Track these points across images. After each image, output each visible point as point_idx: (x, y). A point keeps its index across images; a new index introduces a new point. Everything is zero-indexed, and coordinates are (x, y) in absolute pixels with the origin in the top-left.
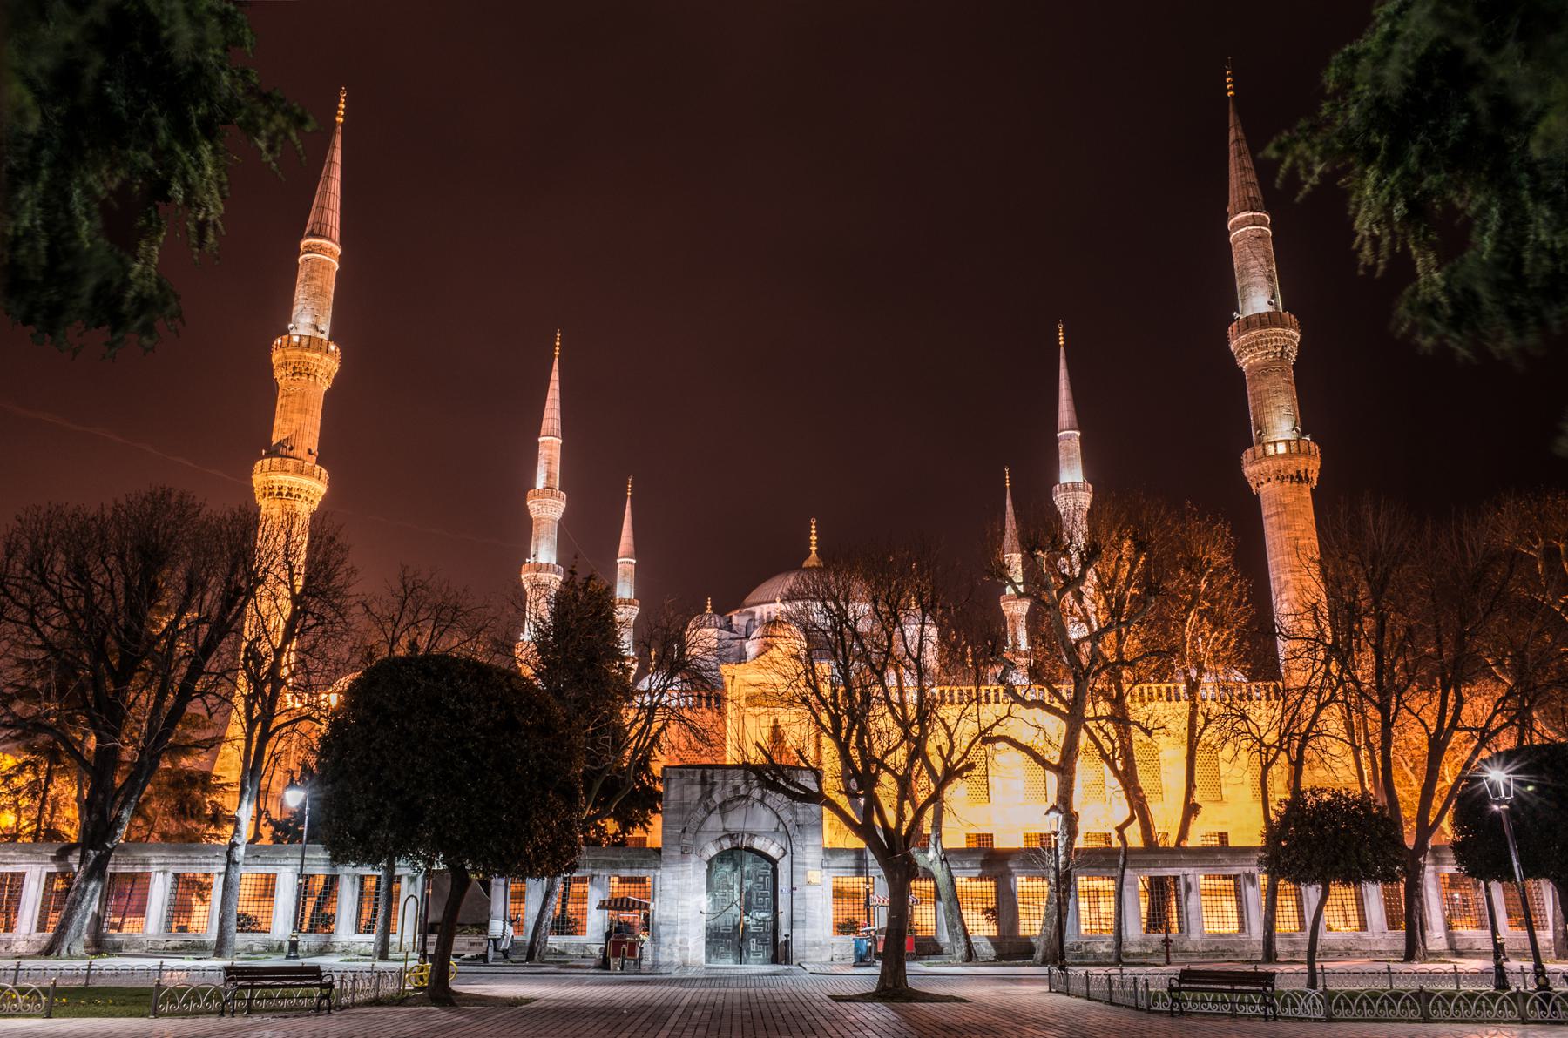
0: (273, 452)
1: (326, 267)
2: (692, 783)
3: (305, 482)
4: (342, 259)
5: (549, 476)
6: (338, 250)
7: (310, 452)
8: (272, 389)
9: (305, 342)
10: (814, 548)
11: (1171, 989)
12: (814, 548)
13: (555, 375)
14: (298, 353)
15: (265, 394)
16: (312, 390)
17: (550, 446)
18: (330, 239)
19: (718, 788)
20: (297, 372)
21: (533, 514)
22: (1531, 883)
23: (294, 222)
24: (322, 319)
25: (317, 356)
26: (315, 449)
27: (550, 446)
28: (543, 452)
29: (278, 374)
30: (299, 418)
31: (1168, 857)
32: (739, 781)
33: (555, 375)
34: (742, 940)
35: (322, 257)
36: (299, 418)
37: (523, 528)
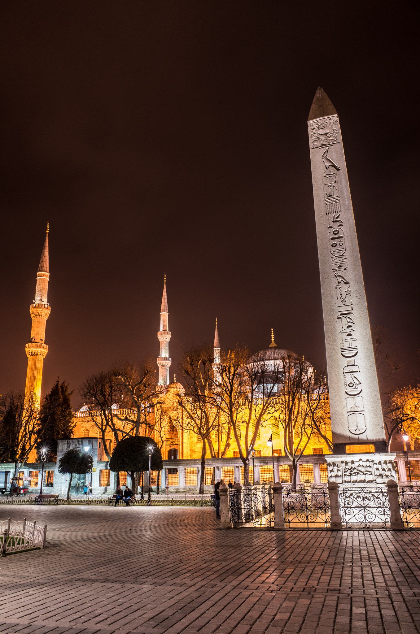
0: (30, 341)
1: (44, 280)
2: (65, 444)
3: (39, 350)
4: (50, 277)
5: (164, 326)
6: (49, 274)
7: (41, 340)
8: (31, 320)
9: (37, 306)
10: (273, 340)
11: (36, 499)
12: (273, 340)
13: (165, 290)
14: (35, 309)
15: (28, 322)
16: (41, 320)
17: (164, 316)
18: (45, 271)
19: (71, 445)
20: (36, 316)
21: (159, 340)
22: (111, 471)
23: (36, 267)
24: (43, 297)
25: (41, 309)
26: (44, 339)
27: (164, 316)
28: (162, 318)
29: (32, 316)
30: (39, 331)
31: (193, 462)
32: (76, 443)
33: (165, 290)
34: (78, 488)
35: (43, 278)
36: (39, 331)
37: (157, 344)
